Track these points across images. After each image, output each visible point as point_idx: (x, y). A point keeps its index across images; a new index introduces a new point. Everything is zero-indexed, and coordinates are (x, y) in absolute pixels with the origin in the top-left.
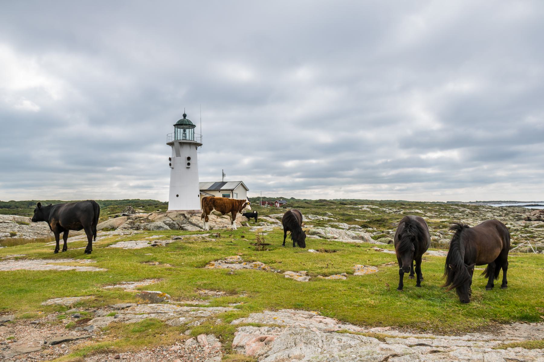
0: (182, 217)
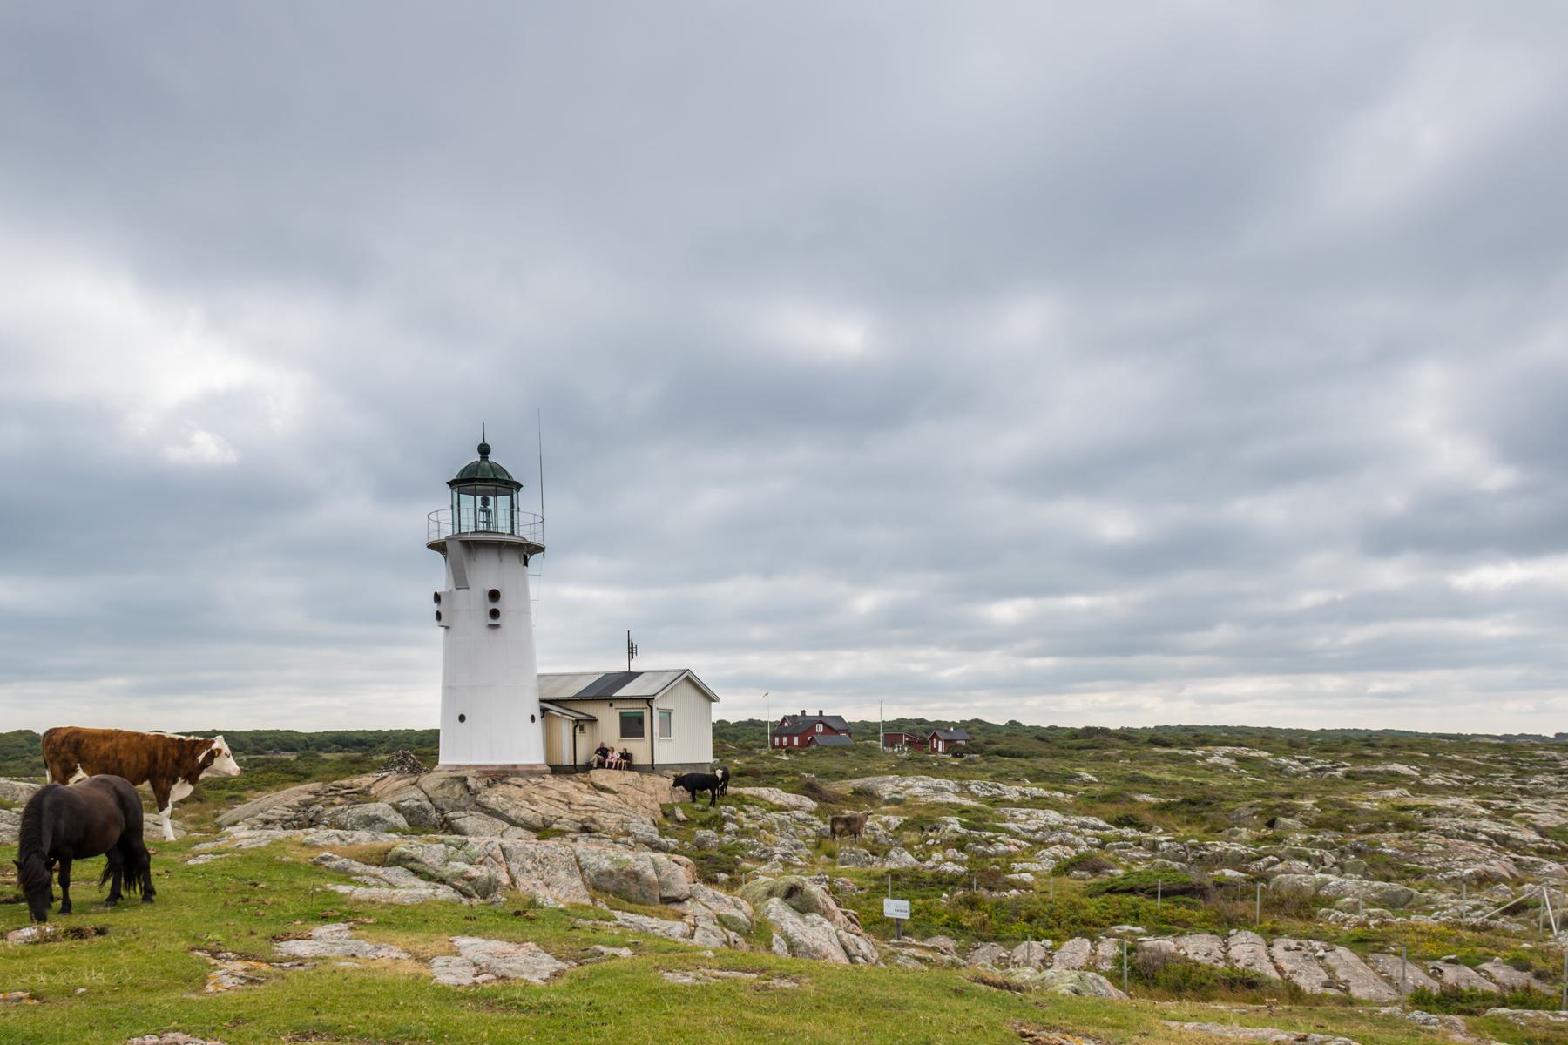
0: (458, 787)
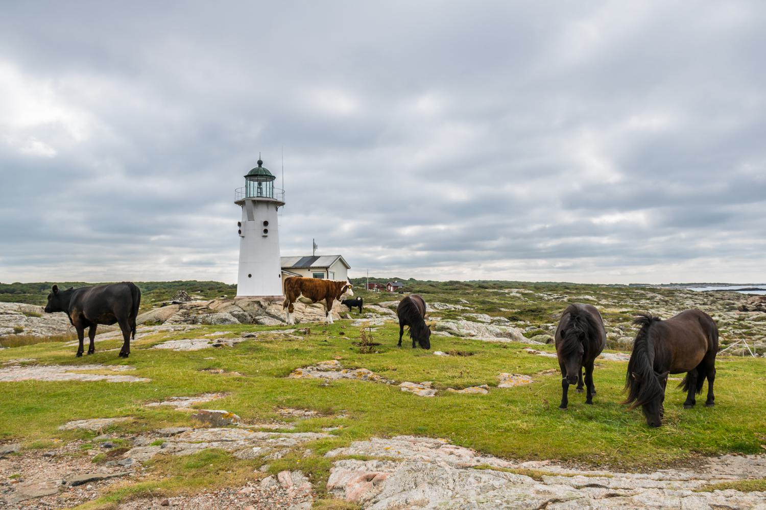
0: (256, 306)
